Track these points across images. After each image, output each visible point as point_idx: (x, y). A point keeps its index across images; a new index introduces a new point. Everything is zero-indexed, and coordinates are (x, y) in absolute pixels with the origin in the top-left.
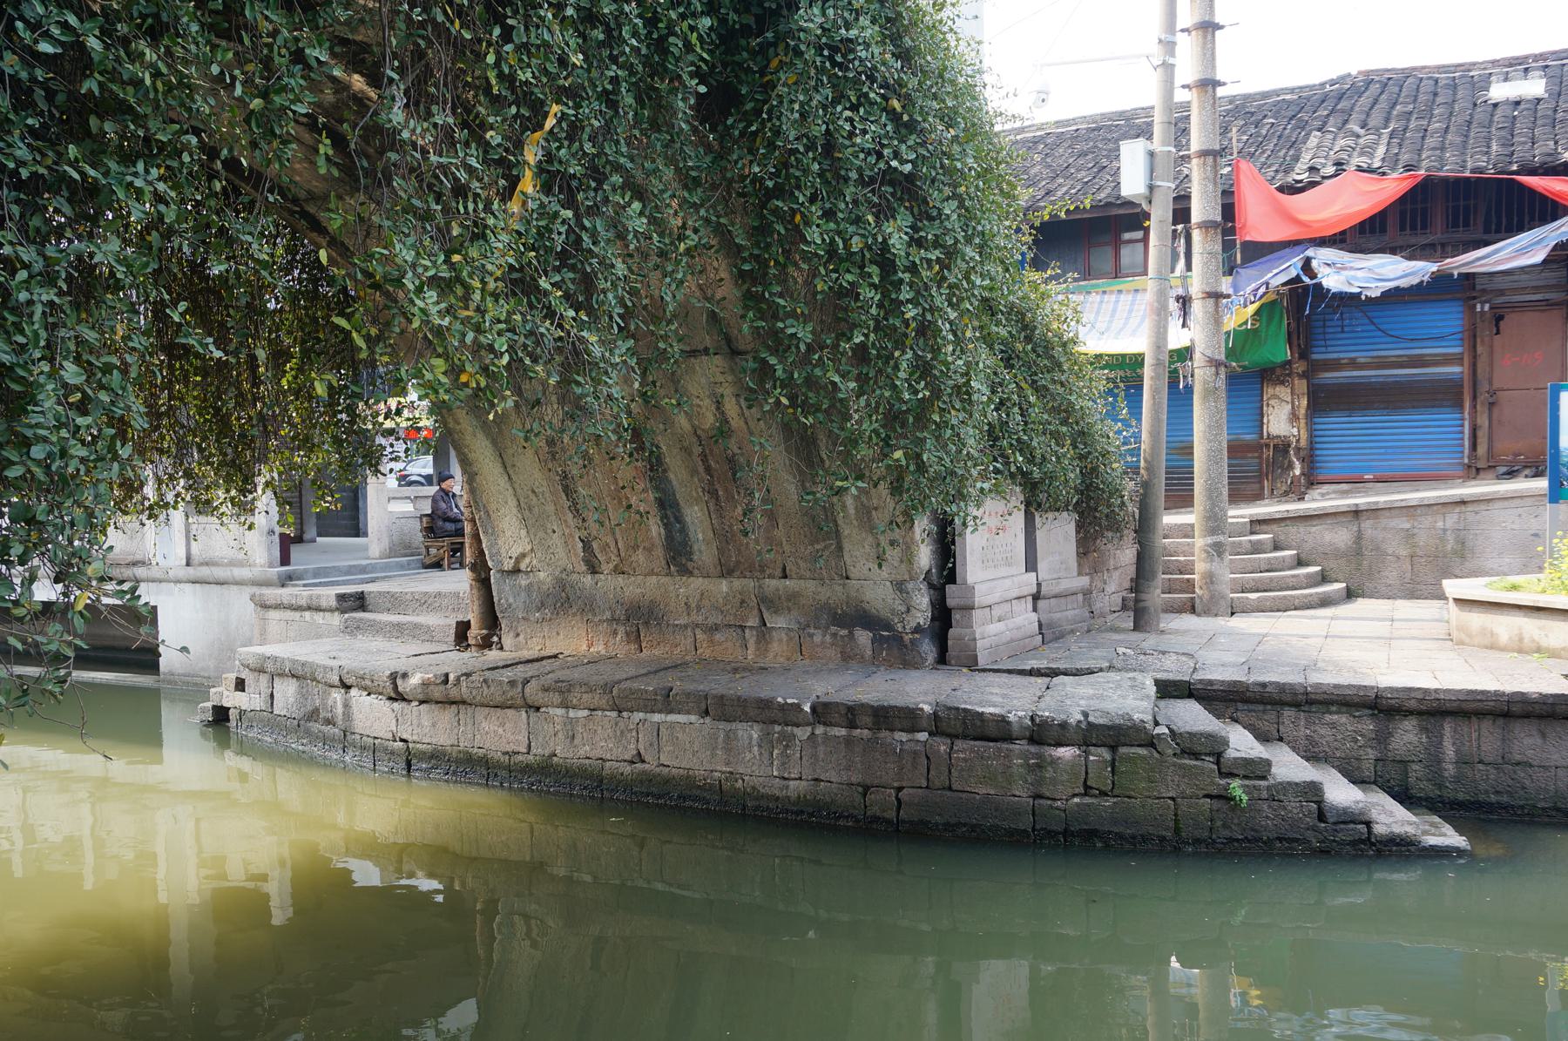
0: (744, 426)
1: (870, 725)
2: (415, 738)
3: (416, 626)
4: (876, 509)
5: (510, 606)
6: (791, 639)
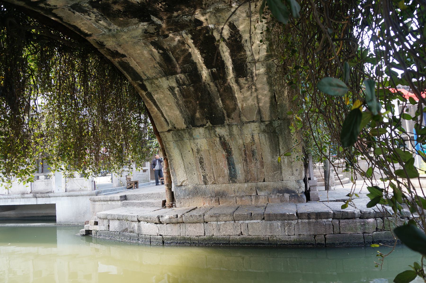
0: (259, 142)
1: (315, 218)
2: (165, 234)
3: (148, 203)
4: (293, 162)
5: (179, 195)
6: (265, 198)
